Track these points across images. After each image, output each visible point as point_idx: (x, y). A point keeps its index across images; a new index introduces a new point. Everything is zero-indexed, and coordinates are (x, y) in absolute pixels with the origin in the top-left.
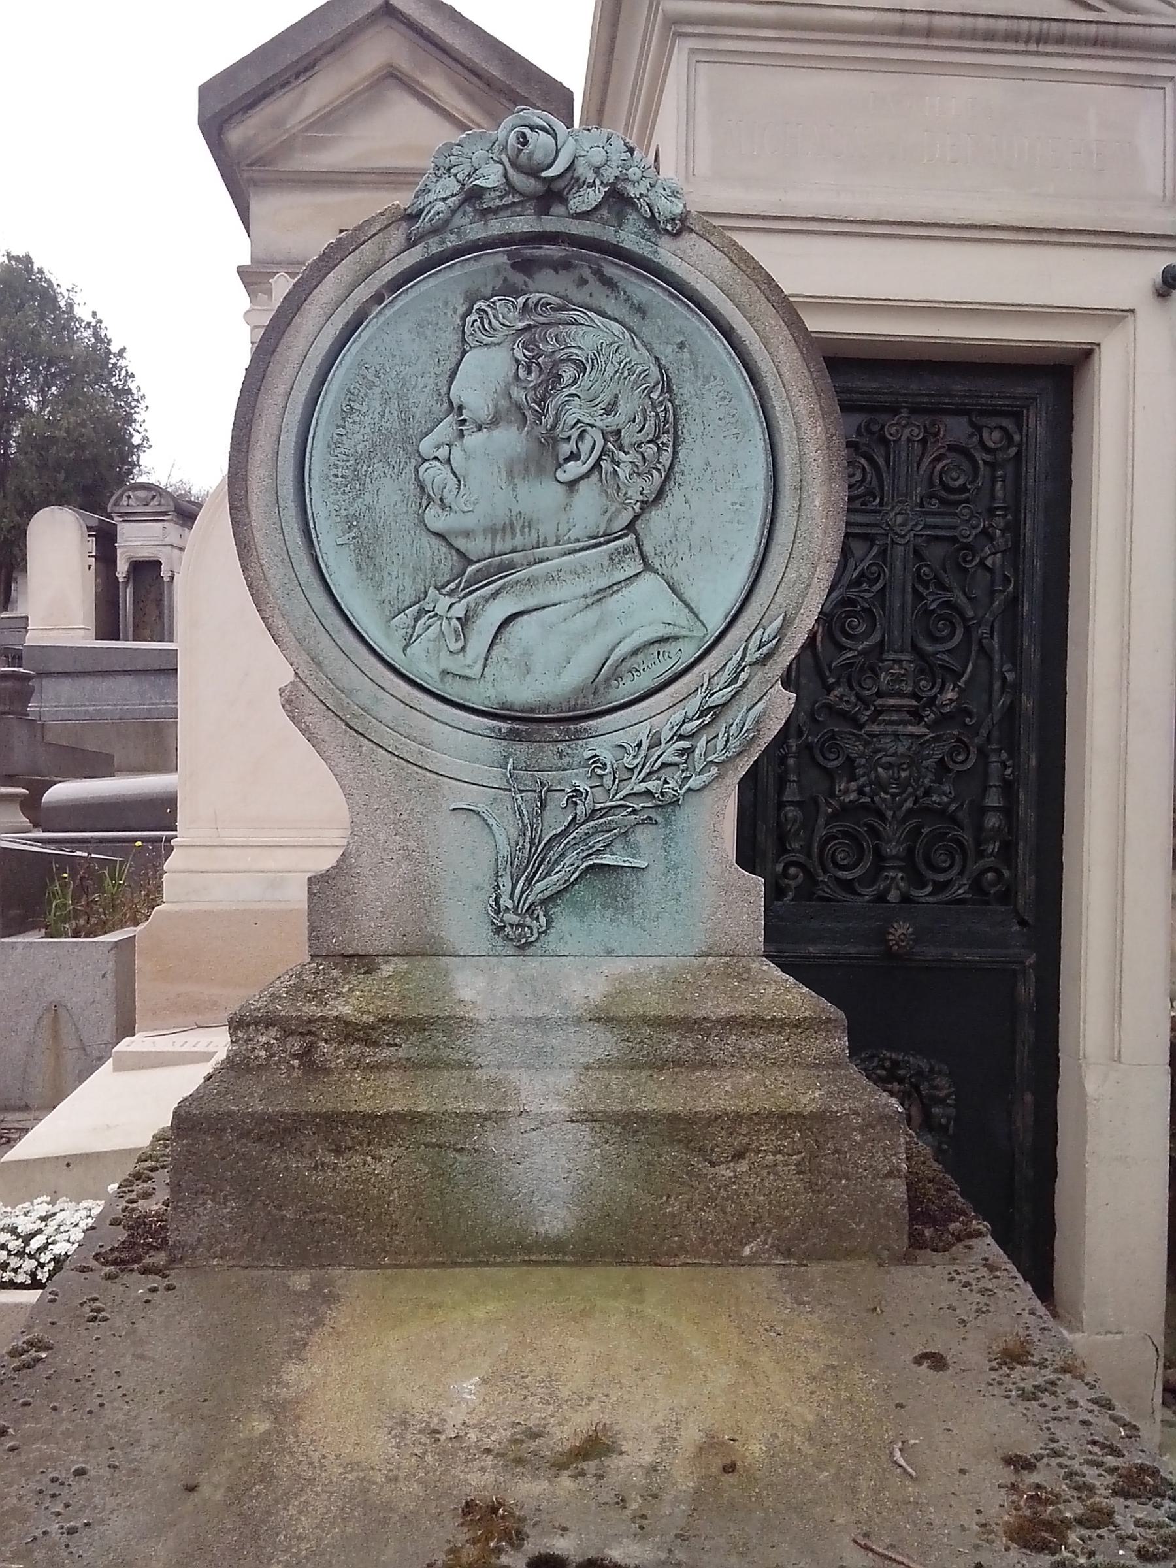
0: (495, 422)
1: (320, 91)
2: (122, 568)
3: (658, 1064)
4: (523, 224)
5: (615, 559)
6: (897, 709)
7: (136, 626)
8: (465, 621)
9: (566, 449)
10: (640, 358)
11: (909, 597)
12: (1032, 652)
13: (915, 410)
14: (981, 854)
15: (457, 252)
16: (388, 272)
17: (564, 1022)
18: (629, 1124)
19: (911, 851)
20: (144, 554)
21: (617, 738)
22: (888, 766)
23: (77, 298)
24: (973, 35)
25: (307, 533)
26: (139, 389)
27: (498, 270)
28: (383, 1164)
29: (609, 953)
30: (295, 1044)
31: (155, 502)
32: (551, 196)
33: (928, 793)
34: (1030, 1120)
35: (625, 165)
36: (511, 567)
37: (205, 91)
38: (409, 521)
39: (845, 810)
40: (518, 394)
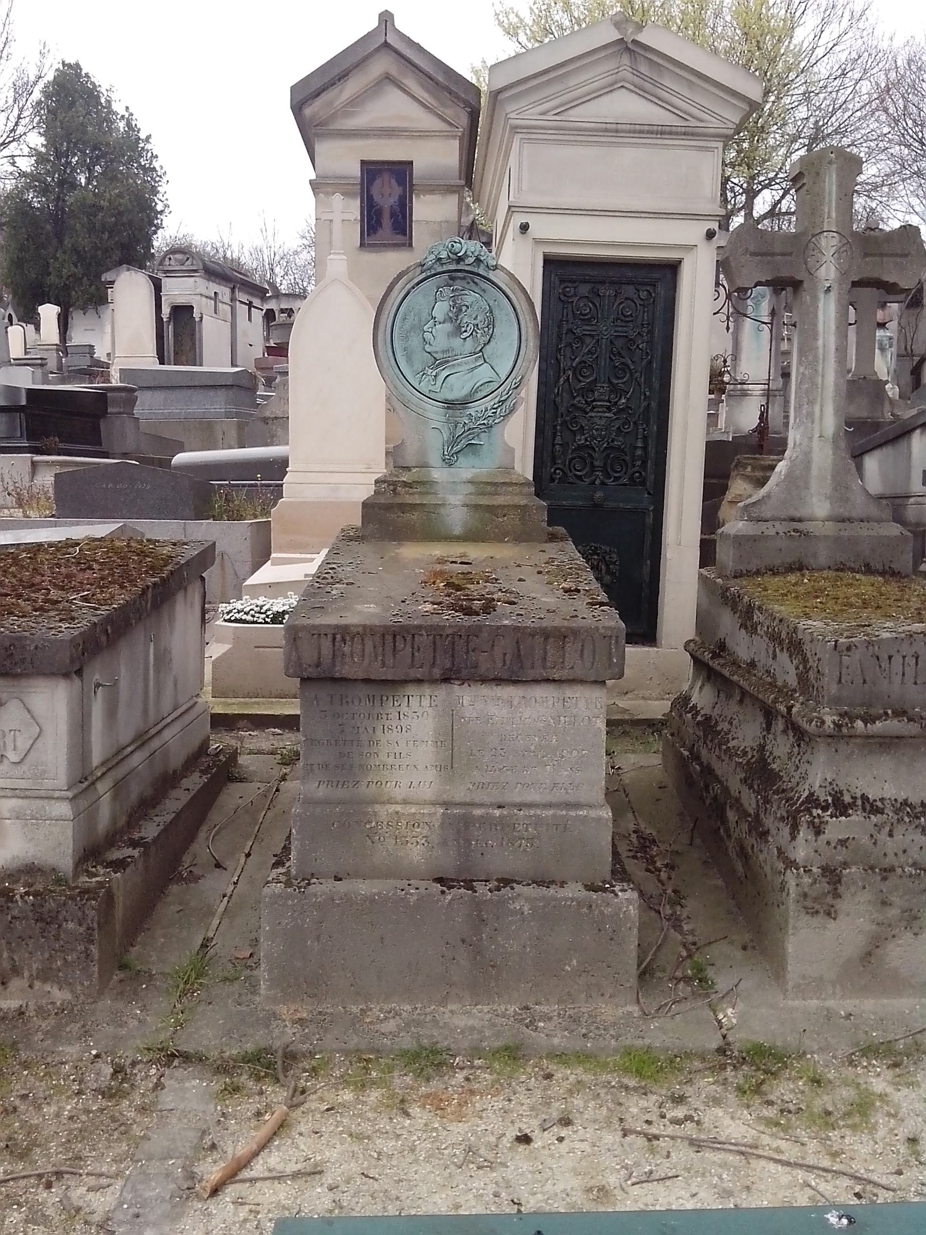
0: (444, 322)
1: (352, 87)
2: (166, 311)
3: (483, 494)
4: (453, 267)
5: (476, 359)
6: (602, 406)
7: (176, 353)
8: (435, 376)
9: (463, 329)
10: (484, 304)
11: (608, 360)
12: (656, 385)
13: (612, 283)
14: (634, 466)
15: (435, 275)
16: (416, 281)
17: (460, 483)
18: (477, 507)
19: (605, 464)
20: (181, 301)
21: (476, 409)
22: (597, 430)
23: (114, 96)
24: (635, 132)
25: (393, 352)
26: (162, 168)
27: (446, 280)
28: (415, 516)
29: (473, 467)
30: (392, 487)
31: (188, 262)
32: (460, 260)
33: (613, 441)
34: (648, 570)
35: (480, 251)
36: (448, 362)
37: (294, 89)
38: (420, 349)
39: (580, 447)
40: (451, 315)
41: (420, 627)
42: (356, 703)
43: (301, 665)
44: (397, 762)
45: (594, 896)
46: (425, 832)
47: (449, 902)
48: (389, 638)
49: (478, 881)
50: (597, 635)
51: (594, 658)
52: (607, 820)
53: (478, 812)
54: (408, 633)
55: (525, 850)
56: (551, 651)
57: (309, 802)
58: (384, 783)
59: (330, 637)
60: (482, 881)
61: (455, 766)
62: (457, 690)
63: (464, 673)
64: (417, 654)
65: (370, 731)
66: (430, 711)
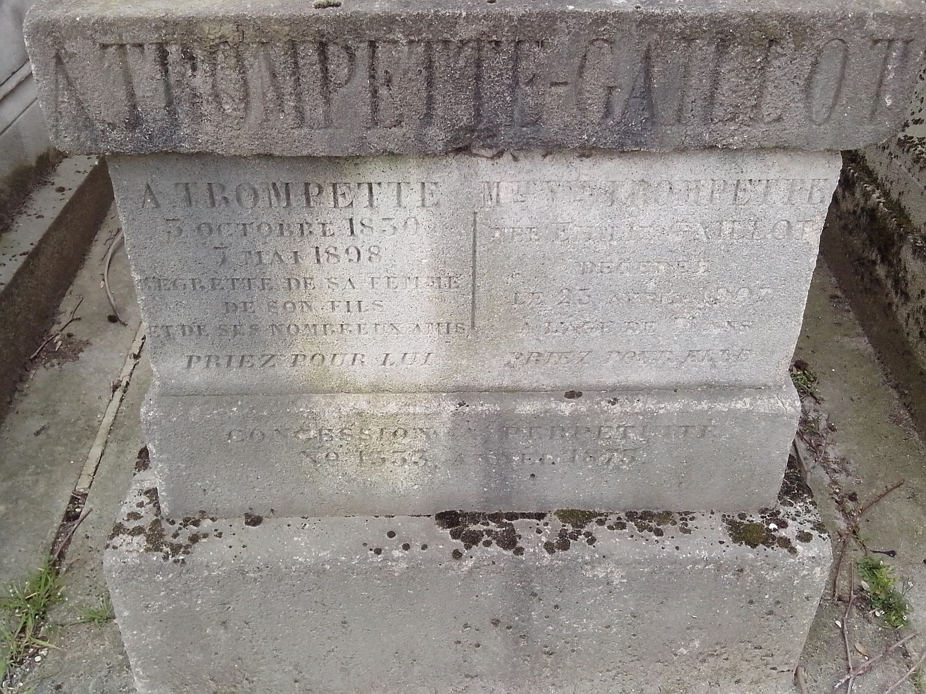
41: (389, 21)
42: (249, 203)
43: (89, 124)
44: (354, 318)
45: (749, 553)
46: (419, 445)
47: (470, 571)
48: (309, 53)
49: (523, 515)
50: (857, 37)
51: (837, 96)
52: (792, 417)
53: (526, 408)
54: (359, 37)
55: (617, 468)
56: (730, 80)
57: (174, 395)
58: (328, 358)
59: (151, 52)
60: (529, 516)
61: (480, 323)
62: (484, 169)
63: (505, 134)
64: (383, 92)
65: (288, 258)
66: (422, 215)
